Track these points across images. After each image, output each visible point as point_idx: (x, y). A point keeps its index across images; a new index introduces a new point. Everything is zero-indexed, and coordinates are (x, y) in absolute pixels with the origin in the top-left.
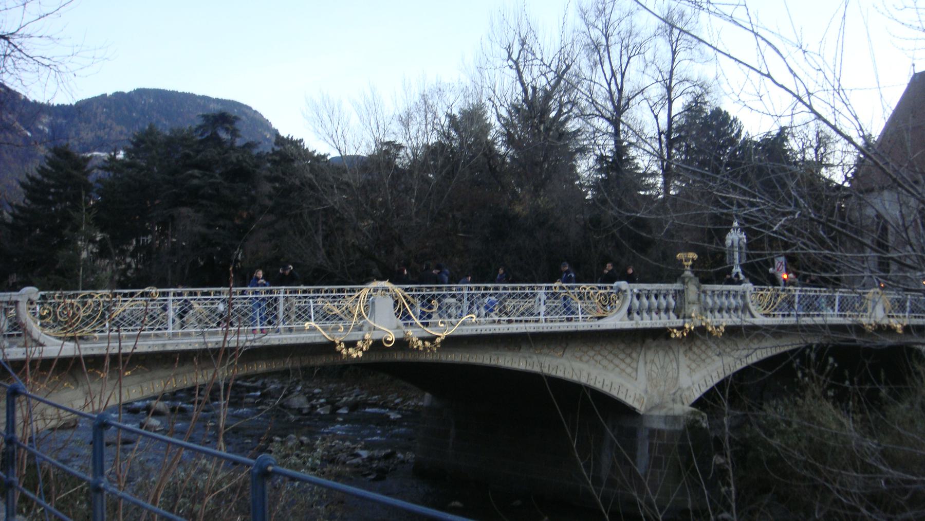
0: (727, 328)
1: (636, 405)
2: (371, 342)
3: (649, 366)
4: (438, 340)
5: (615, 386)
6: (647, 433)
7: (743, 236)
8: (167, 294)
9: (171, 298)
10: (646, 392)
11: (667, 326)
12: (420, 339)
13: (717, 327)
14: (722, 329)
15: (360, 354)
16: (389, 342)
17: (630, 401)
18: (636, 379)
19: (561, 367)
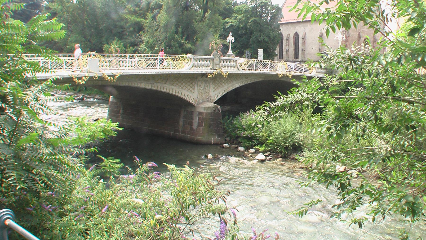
0: (229, 73)
1: (193, 102)
2: (88, 77)
3: (199, 87)
4: (117, 77)
5: (186, 95)
6: (198, 113)
7: (233, 38)
10: (198, 97)
11: (207, 72)
12: (109, 76)
13: (226, 73)
14: (227, 74)
15: (84, 82)
16: (96, 77)
17: (191, 101)
18: (194, 93)
19: (165, 88)
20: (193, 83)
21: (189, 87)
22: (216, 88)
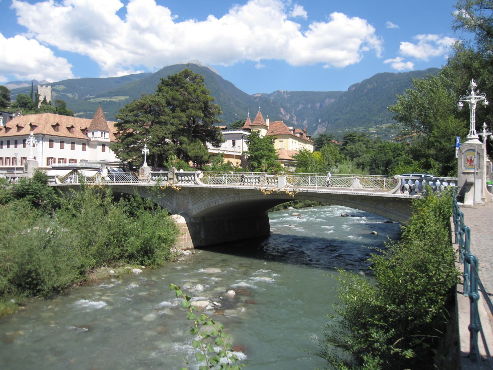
8: (225, 173)
9: (316, 176)
20: (173, 196)
21: (169, 199)
22: (195, 202)
